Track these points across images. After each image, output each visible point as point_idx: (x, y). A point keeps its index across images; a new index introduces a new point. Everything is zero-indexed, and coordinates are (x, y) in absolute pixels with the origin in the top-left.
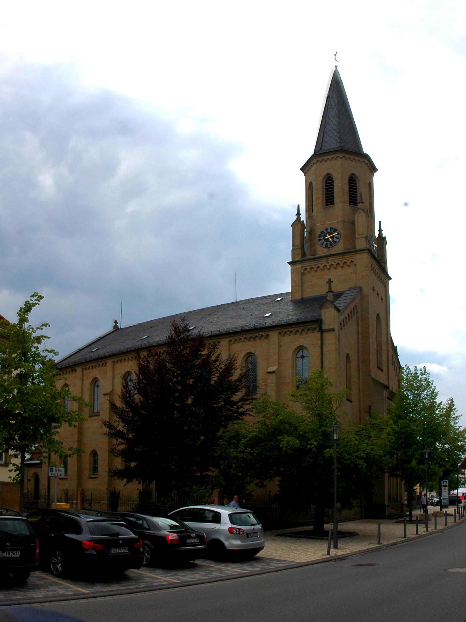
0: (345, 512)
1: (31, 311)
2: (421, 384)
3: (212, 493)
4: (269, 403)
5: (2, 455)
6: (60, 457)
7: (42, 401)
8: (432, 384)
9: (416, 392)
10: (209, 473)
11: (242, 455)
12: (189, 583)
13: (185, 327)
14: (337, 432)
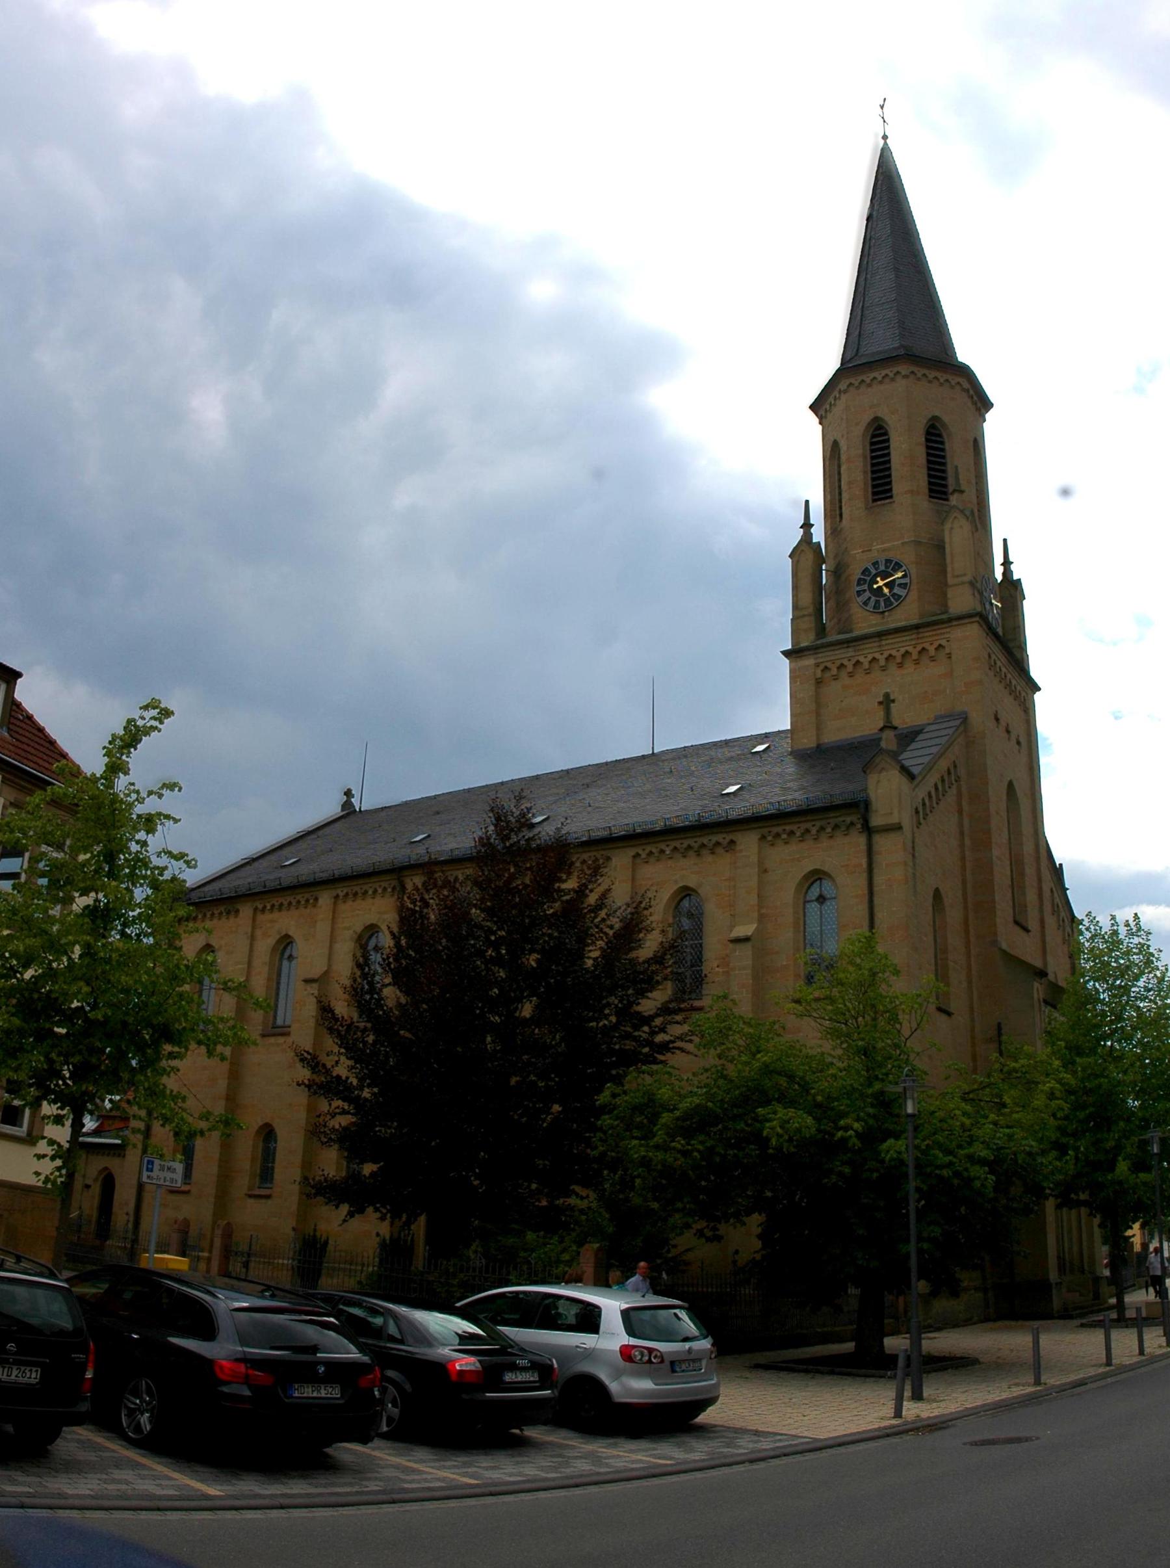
0: (942, 1305)
1: (138, 746)
2: (1129, 960)
3: (579, 1253)
4: (735, 1020)
5: (23, 1112)
6: (176, 1134)
7: (142, 983)
8: (1158, 959)
9: (1118, 982)
10: (573, 1201)
11: (660, 1155)
12: (504, 1488)
13: (524, 817)
14: (916, 1095)
